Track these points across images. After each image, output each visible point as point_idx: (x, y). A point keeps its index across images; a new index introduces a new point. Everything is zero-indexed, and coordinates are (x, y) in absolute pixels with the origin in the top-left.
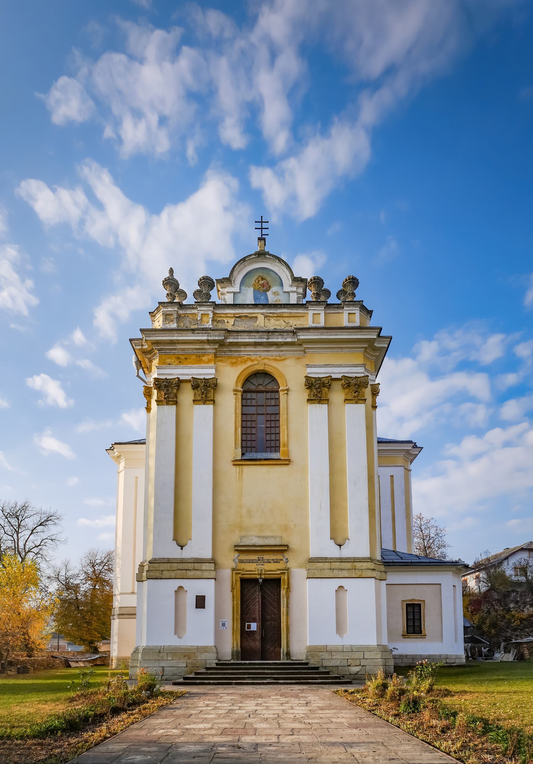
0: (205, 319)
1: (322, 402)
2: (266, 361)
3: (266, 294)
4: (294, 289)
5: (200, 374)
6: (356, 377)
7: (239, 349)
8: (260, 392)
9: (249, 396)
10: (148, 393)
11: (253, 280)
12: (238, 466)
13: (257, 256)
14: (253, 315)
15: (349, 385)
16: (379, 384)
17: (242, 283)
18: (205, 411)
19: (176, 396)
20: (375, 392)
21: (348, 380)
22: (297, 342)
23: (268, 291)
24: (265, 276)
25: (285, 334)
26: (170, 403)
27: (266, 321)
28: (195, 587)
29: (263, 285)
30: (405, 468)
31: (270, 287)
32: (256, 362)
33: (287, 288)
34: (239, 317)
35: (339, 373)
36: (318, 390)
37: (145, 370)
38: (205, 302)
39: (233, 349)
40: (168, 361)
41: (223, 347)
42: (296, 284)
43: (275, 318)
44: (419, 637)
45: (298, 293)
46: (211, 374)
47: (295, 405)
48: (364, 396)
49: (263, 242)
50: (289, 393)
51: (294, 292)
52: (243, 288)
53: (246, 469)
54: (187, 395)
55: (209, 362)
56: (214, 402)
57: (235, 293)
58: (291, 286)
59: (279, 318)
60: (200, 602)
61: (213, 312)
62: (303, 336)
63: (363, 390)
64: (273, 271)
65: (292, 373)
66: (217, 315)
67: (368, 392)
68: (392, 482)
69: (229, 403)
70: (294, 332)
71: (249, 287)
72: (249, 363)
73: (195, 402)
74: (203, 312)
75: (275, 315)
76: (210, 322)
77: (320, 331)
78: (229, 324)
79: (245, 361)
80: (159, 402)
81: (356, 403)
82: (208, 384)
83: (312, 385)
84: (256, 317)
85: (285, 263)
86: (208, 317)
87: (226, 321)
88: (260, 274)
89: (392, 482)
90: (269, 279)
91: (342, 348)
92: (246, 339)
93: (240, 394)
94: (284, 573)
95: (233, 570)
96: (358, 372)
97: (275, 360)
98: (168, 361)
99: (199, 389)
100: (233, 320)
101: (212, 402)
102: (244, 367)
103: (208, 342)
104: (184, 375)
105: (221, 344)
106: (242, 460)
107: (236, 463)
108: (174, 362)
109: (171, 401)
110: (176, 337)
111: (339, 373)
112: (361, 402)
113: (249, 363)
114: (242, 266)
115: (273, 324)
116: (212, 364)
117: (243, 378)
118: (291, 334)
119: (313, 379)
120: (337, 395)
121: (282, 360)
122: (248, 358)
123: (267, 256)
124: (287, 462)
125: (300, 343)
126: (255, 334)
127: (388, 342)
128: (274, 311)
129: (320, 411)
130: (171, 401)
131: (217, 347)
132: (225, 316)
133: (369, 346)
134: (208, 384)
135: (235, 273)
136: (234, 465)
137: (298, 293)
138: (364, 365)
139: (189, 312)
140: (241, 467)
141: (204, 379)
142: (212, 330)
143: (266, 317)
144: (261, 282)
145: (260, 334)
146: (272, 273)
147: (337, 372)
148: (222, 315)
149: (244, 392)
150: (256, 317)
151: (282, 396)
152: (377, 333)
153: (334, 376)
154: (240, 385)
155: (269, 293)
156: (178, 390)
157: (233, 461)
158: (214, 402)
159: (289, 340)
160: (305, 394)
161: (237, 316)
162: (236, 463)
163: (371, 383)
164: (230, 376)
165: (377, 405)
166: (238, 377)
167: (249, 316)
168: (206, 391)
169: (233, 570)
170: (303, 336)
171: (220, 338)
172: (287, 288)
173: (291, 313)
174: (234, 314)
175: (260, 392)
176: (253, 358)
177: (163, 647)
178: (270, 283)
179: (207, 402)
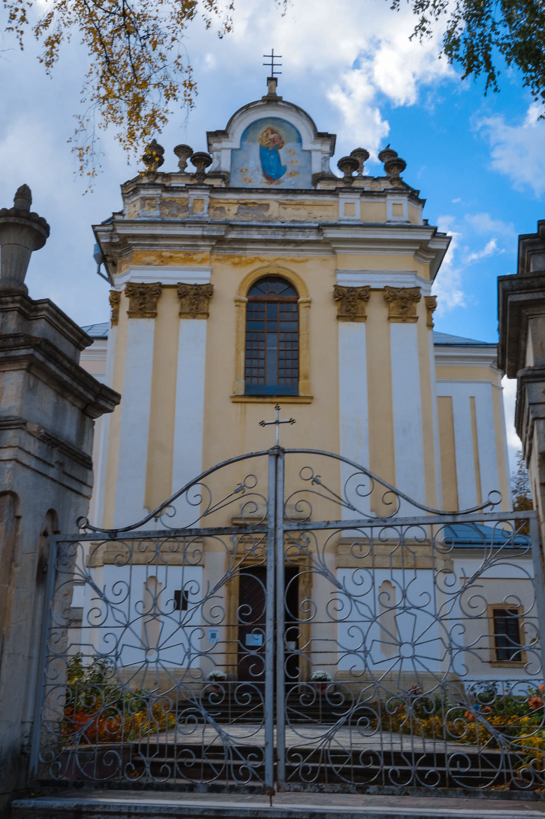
0: (198, 205)
1: (357, 319)
2: (281, 263)
3: (277, 152)
4: (318, 146)
5: (190, 279)
6: (403, 289)
7: (244, 247)
8: (272, 305)
9: (255, 306)
10: (115, 300)
11: (260, 133)
12: (239, 404)
13: (265, 103)
14: (263, 202)
15: (394, 298)
16: (435, 297)
17: (245, 136)
18: (194, 327)
19: (155, 307)
20: (431, 305)
21: (393, 292)
22: (323, 239)
23: (281, 148)
24: (276, 128)
25: (307, 230)
26: (148, 315)
27: (282, 210)
28: (173, 578)
29: (273, 140)
30: (493, 385)
31: (283, 143)
32: (266, 264)
33: (307, 146)
34: (245, 204)
35: (380, 282)
36: (350, 303)
37: (110, 265)
38: (200, 185)
39: (236, 246)
40: (148, 259)
41: (223, 241)
42: (320, 141)
43: (293, 207)
44: (517, 666)
45: (323, 152)
46: (205, 279)
47: (318, 316)
48: (415, 313)
49: (273, 83)
50: (312, 305)
51: (318, 150)
52: (245, 143)
53: (249, 406)
54: (169, 305)
55: (203, 261)
56: (207, 315)
57: (233, 150)
58: (313, 143)
59: (298, 206)
60: (181, 600)
61: (209, 197)
62: (330, 234)
63: (414, 305)
64: (288, 123)
65: (316, 278)
66: (214, 201)
67: (420, 308)
68: (473, 407)
69: (228, 317)
70: (320, 228)
71: (254, 141)
72: (257, 265)
73: (182, 316)
74: (195, 197)
75: (294, 203)
76: (206, 210)
77: (355, 228)
78: (230, 212)
79: (252, 262)
80: (131, 314)
81: (404, 321)
82: (201, 292)
83: (344, 296)
84: (268, 205)
85: (305, 113)
86: (203, 203)
87: (226, 208)
88: (270, 126)
89: (473, 407)
90: (282, 132)
91: (384, 250)
92: (255, 235)
93: (244, 305)
94: (304, 560)
95: (231, 552)
96: (406, 282)
97: (292, 261)
98: (148, 259)
99: (188, 297)
100: (237, 206)
101: (206, 316)
102: (249, 269)
103: (203, 238)
104: (167, 278)
105: (220, 240)
106: (245, 396)
107: (236, 399)
108: (155, 261)
109: (149, 313)
110: (159, 230)
111: (380, 282)
112: (411, 320)
113: (257, 265)
114: (245, 115)
115: (289, 215)
116: (206, 265)
117: (248, 284)
118: (315, 231)
119: (345, 289)
120: (376, 310)
121: (302, 261)
122: (255, 258)
123: (280, 103)
124: (309, 400)
125: (328, 242)
126: (267, 229)
127: (446, 243)
128: (292, 198)
129: (352, 330)
130: (149, 313)
131: (214, 243)
132: (226, 201)
133: (421, 248)
134: (201, 292)
135: (234, 124)
136: (234, 402)
137: (323, 152)
138: (415, 273)
139: (176, 195)
140: (243, 405)
141: (195, 285)
142: (209, 224)
143: (281, 204)
144: (271, 136)
145: (274, 229)
146: (286, 124)
147: (377, 281)
148: (221, 201)
149: (250, 302)
150: (268, 205)
151: (302, 311)
152: (431, 234)
153: (373, 286)
154: (244, 292)
155: (281, 152)
156: (158, 298)
157: (232, 397)
158: (207, 315)
159: (313, 237)
160: (333, 310)
161: (243, 202)
162: (236, 399)
163: (423, 294)
164: (230, 280)
165: (434, 321)
166: (242, 283)
167: (258, 202)
168: (196, 300)
169: (231, 552)
170: (330, 234)
171: (219, 234)
172: (307, 146)
173: (314, 201)
174: (239, 200)
175: (272, 305)
176: (263, 257)
177: (85, 490)
178: (284, 138)
179: (199, 316)
